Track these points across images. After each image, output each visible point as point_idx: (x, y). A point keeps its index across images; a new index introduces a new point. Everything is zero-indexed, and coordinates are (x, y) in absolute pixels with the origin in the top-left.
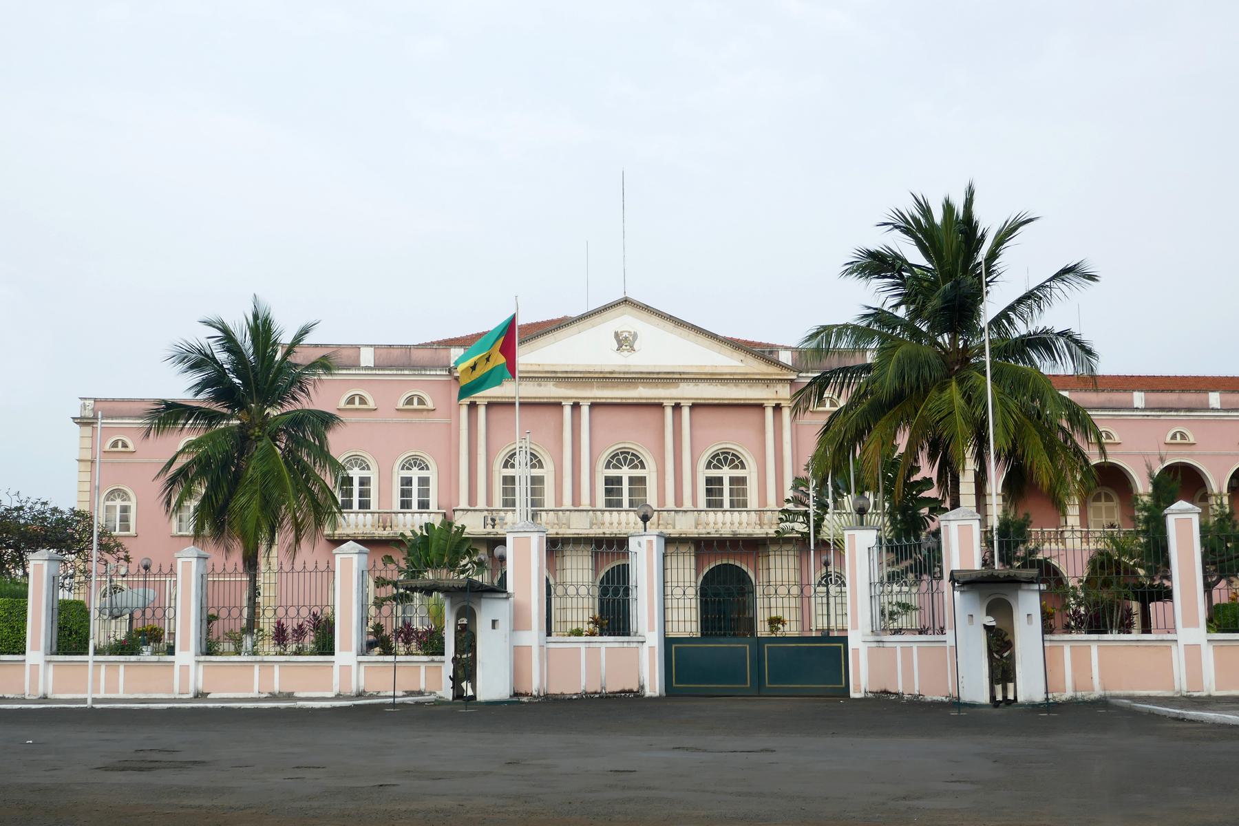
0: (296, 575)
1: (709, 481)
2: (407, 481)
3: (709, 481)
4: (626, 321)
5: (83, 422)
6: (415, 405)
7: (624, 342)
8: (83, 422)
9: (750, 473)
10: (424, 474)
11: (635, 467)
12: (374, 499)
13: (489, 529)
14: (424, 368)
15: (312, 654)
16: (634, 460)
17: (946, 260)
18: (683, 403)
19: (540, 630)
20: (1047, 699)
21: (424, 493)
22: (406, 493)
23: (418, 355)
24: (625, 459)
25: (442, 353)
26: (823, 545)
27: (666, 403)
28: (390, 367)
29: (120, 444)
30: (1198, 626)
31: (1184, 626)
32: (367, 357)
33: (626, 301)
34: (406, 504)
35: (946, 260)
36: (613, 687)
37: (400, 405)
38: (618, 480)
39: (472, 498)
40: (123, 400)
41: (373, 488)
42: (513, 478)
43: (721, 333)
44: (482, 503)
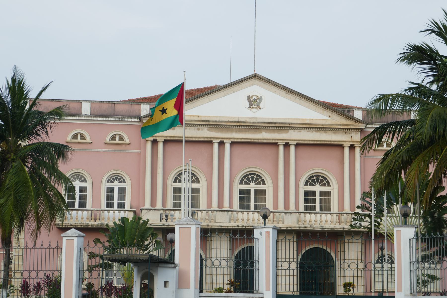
0: (52, 250)
2: (111, 190)
4: (255, 89)
6: (117, 141)
7: (254, 103)
10: (122, 185)
13: (164, 222)
14: (124, 116)
16: (260, 180)
19: (195, 288)
25: (136, 107)
27: (280, 142)
29: (79, 136)
32: (86, 109)
33: (255, 76)
37: (107, 140)
38: (313, 193)
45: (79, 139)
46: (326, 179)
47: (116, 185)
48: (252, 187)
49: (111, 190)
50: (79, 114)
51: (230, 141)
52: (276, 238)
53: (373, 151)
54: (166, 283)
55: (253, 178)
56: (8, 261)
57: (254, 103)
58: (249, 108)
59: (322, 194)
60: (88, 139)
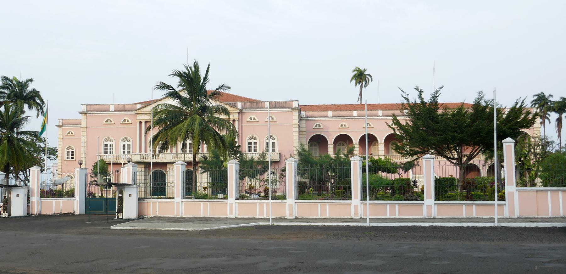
0: (441, 167)
2: (250, 144)
5: (59, 126)
6: (126, 122)
8: (59, 126)
10: (129, 143)
12: (258, 149)
13: (142, 160)
14: (128, 111)
16: (129, 141)
17: (192, 80)
19: (37, 196)
21: (129, 149)
22: (106, 149)
23: (127, 107)
25: (134, 106)
28: (119, 111)
30: (513, 185)
31: (508, 185)
32: (112, 108)
34: (106, 153)
35: (192, 80)
36: (64, 212)
37: (104, 122)
39: (140, 151)
40: (71, 120)
41: (258, 145)
43: (131, 103)
44: (143, 152)
45: (109, 122)
47: (126, 143)
49: (250, 144)
50: (109, 111)
60: (257, 120)
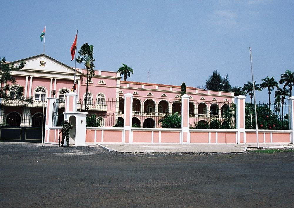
1: (36, 94)
3: (36, 94)
4: (43, 59)
6: (102, 83)
7: (42, 64)
9: (46, 94)
10: (90, 97)
11: (43, 92)
15: (195, 128)
18: (55, 78)
20: (251, 103)
24: (41, 90)
26: (263, 110)
27: (51, 78)
29: (102, 82)
33: (43, 55)
38: (39, 95)
42: (91, 98)
46: (44, 90)
48: (40, 93)
51: (32, 77)
52: (244, 96)
53: (258, 84)
54: (82, 121)
55: (41, 90)
56: (270, 96)
57: (42, 64)
58: (41, 65)
59: (42, 95)
